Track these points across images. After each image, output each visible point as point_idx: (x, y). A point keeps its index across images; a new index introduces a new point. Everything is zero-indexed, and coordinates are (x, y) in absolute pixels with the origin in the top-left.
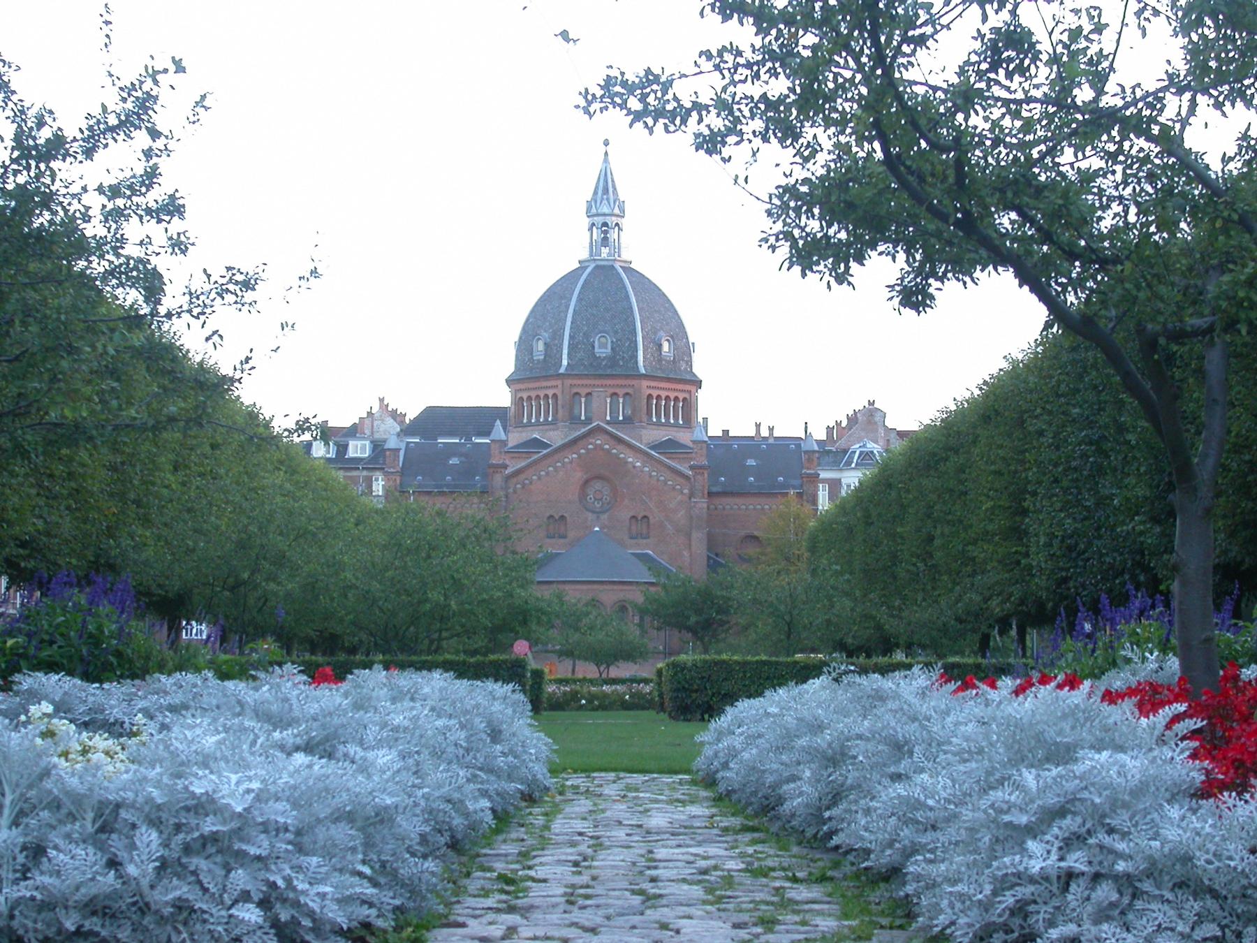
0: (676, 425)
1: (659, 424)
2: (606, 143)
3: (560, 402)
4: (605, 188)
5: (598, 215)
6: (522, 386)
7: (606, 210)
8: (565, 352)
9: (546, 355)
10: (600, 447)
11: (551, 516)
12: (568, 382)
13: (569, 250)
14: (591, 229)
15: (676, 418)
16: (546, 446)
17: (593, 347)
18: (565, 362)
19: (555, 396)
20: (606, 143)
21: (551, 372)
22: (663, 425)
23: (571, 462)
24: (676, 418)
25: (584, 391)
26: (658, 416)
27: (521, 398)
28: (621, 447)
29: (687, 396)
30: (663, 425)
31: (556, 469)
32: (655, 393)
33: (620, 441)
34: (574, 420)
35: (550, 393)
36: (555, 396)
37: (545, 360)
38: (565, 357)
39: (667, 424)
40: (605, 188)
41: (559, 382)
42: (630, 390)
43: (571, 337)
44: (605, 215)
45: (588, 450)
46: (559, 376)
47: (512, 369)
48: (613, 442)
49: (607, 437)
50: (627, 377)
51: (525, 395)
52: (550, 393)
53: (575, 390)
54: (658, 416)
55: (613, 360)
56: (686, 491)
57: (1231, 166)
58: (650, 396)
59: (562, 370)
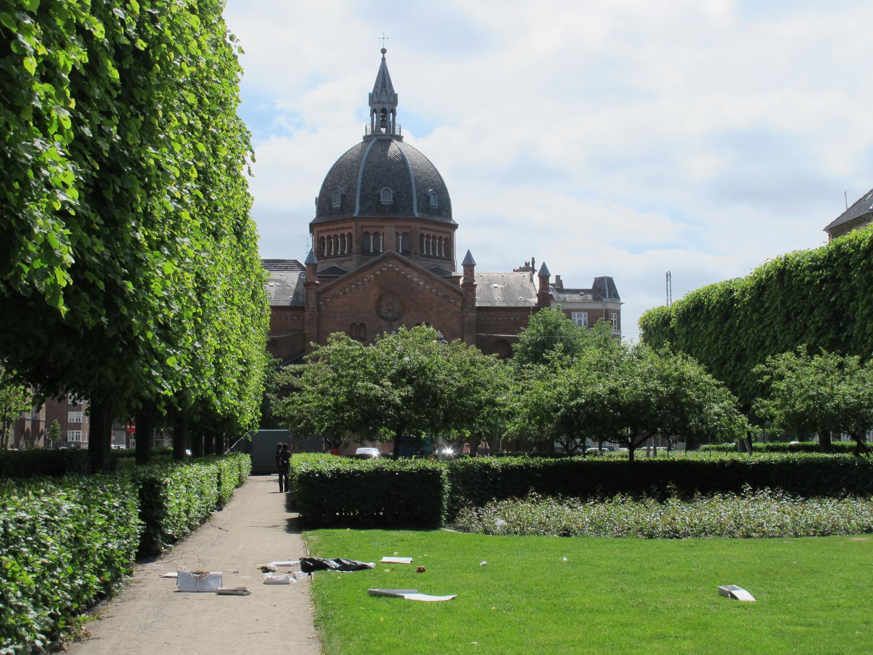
0: (440, 258)
1: (428, 256)
2: (384, 51)
3: (354, 239)
4: (384, 81)
5: (378, 103)
6: (323, 228)
7: (384, 99)
8: (358, 200)
9: (342, 204)
10: (392, 269)
11: (353, 324)
12: (361, 223)
13: (351, 131)
14: (372, 115)
15: (440, 252)
16: (343, 272)
17: (379, 198)
18: (358, 208)
19: (350, 235)
20: (384, 51)
21: (347, 216)
22: (431, 257)
23: (369, 281)
24: (440, 252)
25: (372, 231)
26: (428, 250)
27: (323, 238)
28: (408, 270)
29: (448, 236)
30: (431, 257)
31: (357, 286)
32: (426, 233)
33: (407, 265)
34: (365, 252)
35: (346, 232)
36: (350, 235)
37: (341, 208)
38: (357, 204)
39: (434, 257)
40: (384, 81)
41: (353, 224)
42: (407, 230)
43: (362, 190)
44: (383, 103)
45: (382, 271)
46: (354, 219)
47: (397, 108)
48: (401, 266)
49: (398, 262)
50: (406, 220)
51: (325, 235)
52: (346, 232)
53: (365, 230)
54: (428, 250)
55: (394, 208)
56: (459, 304)
57: (73, 497)
58: (422, 235)
59: (356, 214)
